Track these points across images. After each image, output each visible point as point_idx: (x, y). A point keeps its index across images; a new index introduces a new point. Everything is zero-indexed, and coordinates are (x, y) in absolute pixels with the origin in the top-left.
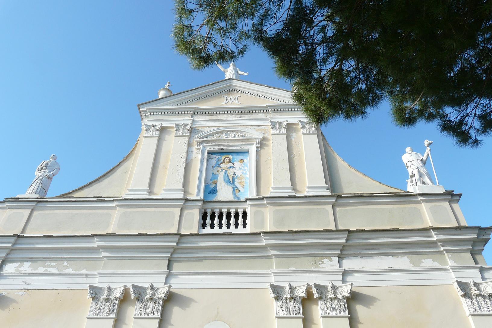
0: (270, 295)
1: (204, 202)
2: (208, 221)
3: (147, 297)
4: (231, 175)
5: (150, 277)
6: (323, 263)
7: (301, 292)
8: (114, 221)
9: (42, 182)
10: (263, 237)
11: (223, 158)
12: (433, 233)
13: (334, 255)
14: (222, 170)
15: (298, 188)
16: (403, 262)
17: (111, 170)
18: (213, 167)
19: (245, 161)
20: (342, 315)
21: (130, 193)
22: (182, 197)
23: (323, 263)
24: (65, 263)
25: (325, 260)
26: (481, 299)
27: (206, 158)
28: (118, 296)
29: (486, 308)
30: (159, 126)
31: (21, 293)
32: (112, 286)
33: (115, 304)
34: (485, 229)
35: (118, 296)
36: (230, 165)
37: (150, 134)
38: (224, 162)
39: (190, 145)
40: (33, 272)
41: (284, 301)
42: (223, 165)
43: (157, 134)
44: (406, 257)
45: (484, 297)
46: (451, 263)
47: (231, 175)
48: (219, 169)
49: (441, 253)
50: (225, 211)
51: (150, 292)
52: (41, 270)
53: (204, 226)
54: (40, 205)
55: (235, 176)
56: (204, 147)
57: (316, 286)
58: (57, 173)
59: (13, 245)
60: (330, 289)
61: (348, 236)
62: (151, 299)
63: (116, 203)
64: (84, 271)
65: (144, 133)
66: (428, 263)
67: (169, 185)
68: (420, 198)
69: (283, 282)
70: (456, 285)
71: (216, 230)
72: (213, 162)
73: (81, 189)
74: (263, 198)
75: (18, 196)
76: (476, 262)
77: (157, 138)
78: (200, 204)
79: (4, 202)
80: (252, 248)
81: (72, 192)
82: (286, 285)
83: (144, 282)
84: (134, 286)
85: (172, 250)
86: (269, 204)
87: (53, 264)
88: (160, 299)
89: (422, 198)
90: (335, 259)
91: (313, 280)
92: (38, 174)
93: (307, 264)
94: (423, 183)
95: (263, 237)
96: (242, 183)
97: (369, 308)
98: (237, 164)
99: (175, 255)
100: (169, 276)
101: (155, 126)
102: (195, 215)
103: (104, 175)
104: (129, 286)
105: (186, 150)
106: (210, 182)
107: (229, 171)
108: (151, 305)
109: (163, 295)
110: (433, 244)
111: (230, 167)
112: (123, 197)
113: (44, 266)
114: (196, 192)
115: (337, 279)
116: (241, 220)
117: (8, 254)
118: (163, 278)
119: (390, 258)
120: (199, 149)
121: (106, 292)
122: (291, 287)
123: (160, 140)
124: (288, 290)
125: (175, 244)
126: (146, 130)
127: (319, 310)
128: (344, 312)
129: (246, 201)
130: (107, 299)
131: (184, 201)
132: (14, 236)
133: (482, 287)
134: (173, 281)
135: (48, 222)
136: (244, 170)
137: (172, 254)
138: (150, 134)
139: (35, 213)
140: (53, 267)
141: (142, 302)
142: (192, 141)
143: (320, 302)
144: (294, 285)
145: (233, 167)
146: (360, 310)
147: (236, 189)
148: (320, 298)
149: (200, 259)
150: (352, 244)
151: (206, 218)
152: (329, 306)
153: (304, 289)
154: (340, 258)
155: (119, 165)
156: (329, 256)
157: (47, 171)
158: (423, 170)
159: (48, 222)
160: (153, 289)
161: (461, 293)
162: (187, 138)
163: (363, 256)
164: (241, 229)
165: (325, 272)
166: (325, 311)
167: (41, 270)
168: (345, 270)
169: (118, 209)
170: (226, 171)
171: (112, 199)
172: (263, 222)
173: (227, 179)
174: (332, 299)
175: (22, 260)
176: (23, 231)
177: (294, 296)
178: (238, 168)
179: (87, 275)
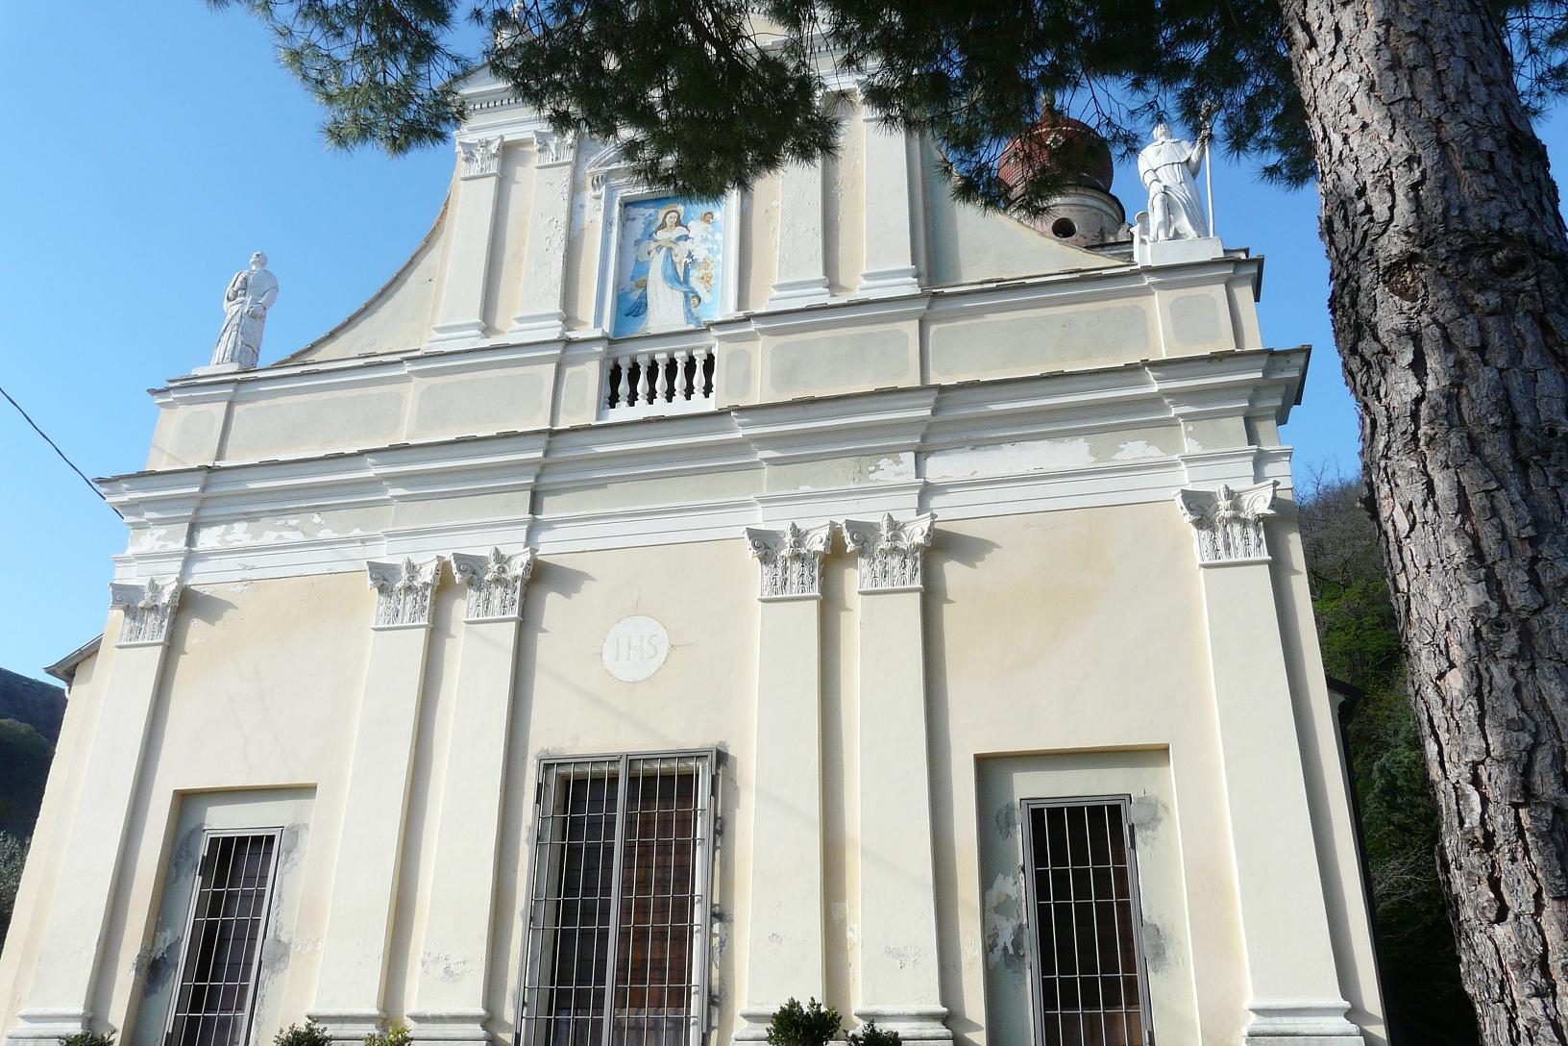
0: (748, 553)
1: (611, 341)
2: (624, 387)
3: (488, 577)
4: (680, 258)
5: (494, 532)
6: (877, 468)
7: (817, 543)
8: (411, 413)
9: (242, 330)
10: (735, 419)
11: (662, 213)
12: (1151, 375)
13: (905, 449)
14: (659, 248)
15: (842, 280)
16: (1074, 453)
17: (396, 279)
18: (637, 243)
19: (717, 215)
20: (907, 586)
21: (439, 336)
22: (555, 337)
23: (877, 468)
24: (316, 518)
25: (884, 463)
26: (1237, 528)
27: (616, 220)
28: (429, 579)
29: (1241, 550)
30: (496, 144)
31: (239, 587)
32: (415, 561)
33: (424, 597)
34: (1287, 353)
35: (429, 579)
36: (680, 231)
37: (475, 169)
38: (663, 226)
39: (576, 189)
40: (254, 542)
41: (780, 564)
42: (661, 235)
43: (494, 167)
44: (1081, 440)
45: (1244, 523)
46: (1190, 447)
47: (680, 258)
48: (653, 245)
49: (1171, 423)
50: (662, 358)
51: (493, 566)
52: (270, 537)
53: (613, 400)
54: (244, 390)
55: (691, 261)
56: (611, 190)
57: (850, 525)
58: (271, 301)
59: (203, 489)
60: (884, 531)
61: (938, 401)
62: (497, 581)
63: (408, 367)
64: (357, 532)
65: (462, 169)
66: (1135, 449)
67: (530, 308)
68: (1148, 280)
69: (775, 520)
70: (1179, 502)
71: (642, 410)
72: (638, 228)
73: (332, 335)
74: (747, 319)
75: (194, 372)
76: (1252, 438)
77: (493, 179)
78: (599, 348)
79: (167, 390)
80: (708, 453)
81: (314, 347)
82: (786, 527)
83: (479, 545)
84: (457, 557)
85: (536, 469)
86: (763, 331)
87: (293, 522)
88: (516, 579)
89: (1153, 279)
90: (909, 458)
91: (844, 512)
92: (231, 309)
93: (839, 474)
94: (1177, 235)
95: (735, 419)
96: (706, 279)
97: (973, 566)
98: (696, 227)
99: (545, 480)
100: (533, 528)
101: (488, 143)
102: (588, 377)
103: (380, 295)
104: (448, 557)
105: (565, 205)
106: (629, 284)
107: (677, 250)
108: (498, 592)
109: (520, 571)
110: (1153, 402)
111: (679, 239)
112: (427, 347)
113: (274, 528)
114: (593, 322)
115: (904, 506)
116: (699, 378)
117: (198, 509)
118: (521, 534)
119: (1043, 445)
120: (598, 198)
121: (404, 575)
122: (796, 532)
123: (503, 182)
124: (789, 539)
125: (540, 454)
126: (467, 160)
127: (856, 578)
128: (912, 579)
129: (708, 329)
130: (409, 589)
131: (561, 346)
132: (200, 469)
133: (1246, 500)
134: (543, 537)
135: (277, 429)
136: (715, 242)
137: (537, 477)
138: (475, 169)
139: (239, 410)
140: (295, 528)
141: (479, 589)
142: (581, 175)
143: (862, 562)
144: (802, 526)
145: (686, 238)
146: (954, 573)
147: (691, 297)
148: (862, 552)
149: (601, 484)
150: (953, 415)
151: (617, 381)
152: (878, 568)
153: (825, 533)
154: (921, 455)
155: (410, 263)
156: (893, 452)
157: (249, 299)
158: (1180, 194)
159: (277, 429)
160: (499, 557)
161: (1188, 518)
162: (568, 170)
163: (977, 445)
164: (699, 404)
165: (884, 495)
166: (869, 579)
167: (270, 537)
168: (926, 484)
169: (416, 380)
170: (670, 249)
171: (397, 358)
172: (747, 378)
173: (670, 271)
174: (886, 553)
175: (230, 520)
176: (220, 456)
177: (803, 551)
178: (698, 239)
179: (363, 541)
